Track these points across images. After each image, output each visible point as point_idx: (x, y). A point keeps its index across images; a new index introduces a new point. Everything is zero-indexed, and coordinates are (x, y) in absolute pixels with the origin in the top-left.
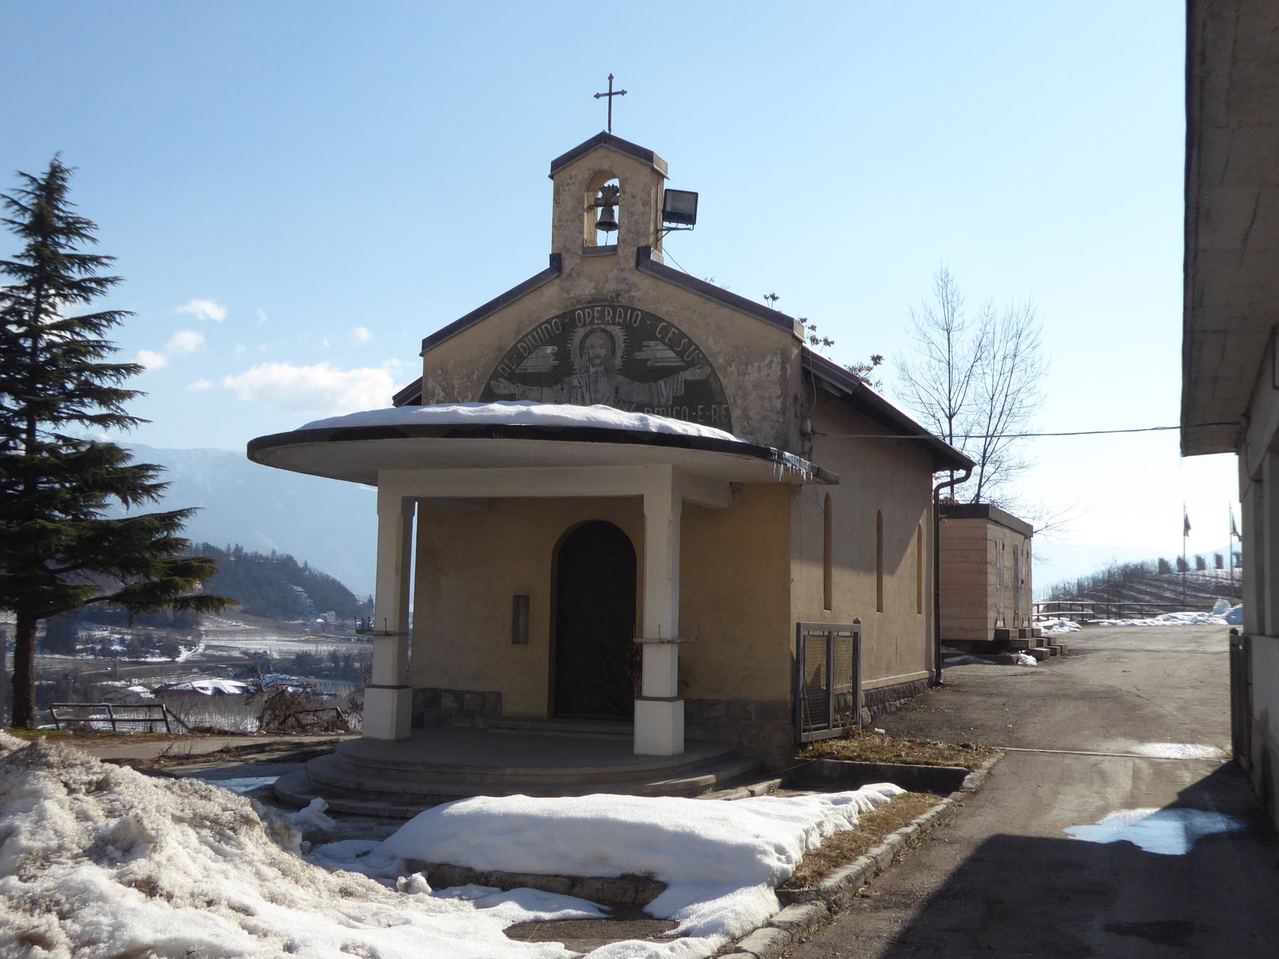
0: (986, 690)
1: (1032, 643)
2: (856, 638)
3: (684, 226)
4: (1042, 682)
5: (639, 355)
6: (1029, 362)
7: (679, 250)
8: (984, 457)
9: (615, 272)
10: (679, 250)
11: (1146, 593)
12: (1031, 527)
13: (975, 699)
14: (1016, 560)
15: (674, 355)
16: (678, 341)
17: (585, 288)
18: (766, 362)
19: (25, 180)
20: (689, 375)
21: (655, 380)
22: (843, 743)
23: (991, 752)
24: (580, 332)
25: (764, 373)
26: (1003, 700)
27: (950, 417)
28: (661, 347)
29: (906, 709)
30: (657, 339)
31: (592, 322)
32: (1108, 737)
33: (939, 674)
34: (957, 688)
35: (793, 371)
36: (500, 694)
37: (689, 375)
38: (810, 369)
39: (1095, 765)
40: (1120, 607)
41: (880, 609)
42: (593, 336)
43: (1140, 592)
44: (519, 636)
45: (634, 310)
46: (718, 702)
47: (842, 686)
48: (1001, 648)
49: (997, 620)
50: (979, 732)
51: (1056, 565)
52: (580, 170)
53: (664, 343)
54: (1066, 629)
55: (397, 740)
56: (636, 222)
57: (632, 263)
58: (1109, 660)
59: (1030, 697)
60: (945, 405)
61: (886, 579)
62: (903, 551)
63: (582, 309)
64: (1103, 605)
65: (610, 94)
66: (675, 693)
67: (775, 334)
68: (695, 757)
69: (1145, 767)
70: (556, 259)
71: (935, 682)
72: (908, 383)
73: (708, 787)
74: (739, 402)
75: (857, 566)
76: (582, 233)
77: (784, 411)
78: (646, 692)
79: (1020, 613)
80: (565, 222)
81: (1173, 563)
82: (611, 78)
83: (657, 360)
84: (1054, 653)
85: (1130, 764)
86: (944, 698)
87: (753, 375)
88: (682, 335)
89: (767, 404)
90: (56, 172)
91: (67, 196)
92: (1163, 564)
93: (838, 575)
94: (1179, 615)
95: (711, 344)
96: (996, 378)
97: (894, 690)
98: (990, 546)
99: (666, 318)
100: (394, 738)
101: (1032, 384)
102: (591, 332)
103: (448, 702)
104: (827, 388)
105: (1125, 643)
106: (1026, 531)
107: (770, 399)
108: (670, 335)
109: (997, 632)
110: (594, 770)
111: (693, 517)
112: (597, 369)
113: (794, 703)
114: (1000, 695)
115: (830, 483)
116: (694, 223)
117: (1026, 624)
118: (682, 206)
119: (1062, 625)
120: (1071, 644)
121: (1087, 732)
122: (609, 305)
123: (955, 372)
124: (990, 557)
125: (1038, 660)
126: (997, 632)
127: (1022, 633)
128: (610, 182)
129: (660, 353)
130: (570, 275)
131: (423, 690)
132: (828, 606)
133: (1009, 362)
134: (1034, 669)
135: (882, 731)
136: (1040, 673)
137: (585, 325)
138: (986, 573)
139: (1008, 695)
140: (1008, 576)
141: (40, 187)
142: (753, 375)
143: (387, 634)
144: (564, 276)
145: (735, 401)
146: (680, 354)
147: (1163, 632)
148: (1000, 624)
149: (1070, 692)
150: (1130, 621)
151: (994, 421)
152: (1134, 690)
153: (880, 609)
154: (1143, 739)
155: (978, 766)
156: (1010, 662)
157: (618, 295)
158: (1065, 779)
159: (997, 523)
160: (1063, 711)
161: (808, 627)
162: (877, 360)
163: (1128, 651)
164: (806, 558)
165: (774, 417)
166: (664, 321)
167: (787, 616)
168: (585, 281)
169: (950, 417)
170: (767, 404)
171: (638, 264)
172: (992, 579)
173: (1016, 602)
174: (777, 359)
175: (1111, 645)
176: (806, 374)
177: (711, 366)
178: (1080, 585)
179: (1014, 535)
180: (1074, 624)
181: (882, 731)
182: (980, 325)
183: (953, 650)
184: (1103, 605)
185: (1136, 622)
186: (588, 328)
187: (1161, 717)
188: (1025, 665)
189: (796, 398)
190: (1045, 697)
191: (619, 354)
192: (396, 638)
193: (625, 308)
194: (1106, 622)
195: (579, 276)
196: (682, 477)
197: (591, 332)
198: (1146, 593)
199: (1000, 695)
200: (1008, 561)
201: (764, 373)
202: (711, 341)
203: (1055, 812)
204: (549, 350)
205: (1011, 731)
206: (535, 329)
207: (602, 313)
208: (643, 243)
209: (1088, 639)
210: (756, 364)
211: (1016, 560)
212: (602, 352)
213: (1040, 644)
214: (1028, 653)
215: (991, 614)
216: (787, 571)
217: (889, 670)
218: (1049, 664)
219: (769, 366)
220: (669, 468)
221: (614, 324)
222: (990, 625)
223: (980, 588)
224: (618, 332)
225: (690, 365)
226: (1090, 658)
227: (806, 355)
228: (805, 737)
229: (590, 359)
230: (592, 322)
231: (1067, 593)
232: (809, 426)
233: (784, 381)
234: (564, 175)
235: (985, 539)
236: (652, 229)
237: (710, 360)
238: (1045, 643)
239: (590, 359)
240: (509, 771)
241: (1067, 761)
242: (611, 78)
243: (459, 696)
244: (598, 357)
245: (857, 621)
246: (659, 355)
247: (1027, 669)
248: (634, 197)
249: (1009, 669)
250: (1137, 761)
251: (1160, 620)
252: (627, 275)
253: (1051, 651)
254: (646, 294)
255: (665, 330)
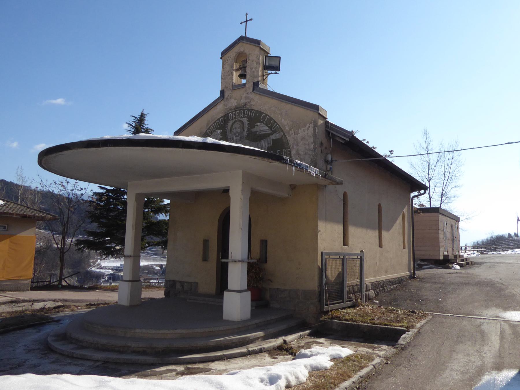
0: (433, 280)
1: (458, 260)
2: (361, 260)
3: (275, 72)
4: (459, 277)
5: (253, 130)
6: (458, 161)
7: (274, 83)
8: (442, 195)
9: (245, 95)
10: (274, 83)
11: (504, 244)
12: (459, 218)
13: (428, 285)
14: (452, 230)
15: (267, 128)
16: (271, 123)
17: (233, 103)
18: (307, 127)
19: (133, 118)
20: (273, 137)
21: (260, 141)
22: (351, 310)
23: (425, 315)
24: (231, 122)
25: (306, 132)
26: (440, 285)
27: (429, 181)
28: (263, 125)
29: (395, 289)
30: (261, 122)
31: (235, 118)
32: (487, 307)
33: (414, 273)
34: (422, 280)
35: (321, 132)
36: (197, 283)
37: (273, 137)
38: (330, 130)
39: (479, 326)
40: (495, 248)
41: (380, 246)
42: (236, 124)
43: (503, 243)
44: (205, 259)
45: (252, 110)
46: (285, 290)
47: (352, 281)
48: (445, 263)
49: (443, 252)
50: (424, 303)
51: (471, 233)
52: (232, 54)
53: (264, 123)
54: (475, 255)
55: (131, 306)
56: (254, 72)
57: (251, 89)
58: (490, 267)
59: (453, 284)
60: (427, 177)
61: (384, 234)
62: (394, 222)
63: (231, 112)
64: (487, 247)
65: (246, 21)
66: (245, 287)
67: (311, 114)
68: (255, 321)
69: (506, 327)
70: (222, 93)
71: (412, 277)
72: (414, 170)
73: (257, 339)
74: (295, 147)
75: (367, 226)
76: (232, 80)
77: (314, 150)
78: (230, 287)
79: (455, 249)
80: (226, 76)
81: (513, 235)
82: (247, 14)
83: (261, 131)
84: (468, 264)
85: (499, 326)
86: (415, 284)
87: (301, 134)
88: (271, 119)
89: (307, 147)
90: (142, 115)
91: (146, 122)
92: (510, 235)
93: (352, 230)
94: (517, 250)
95: (284, 122)
96: (446, 167)
97: (390, 282)
98: (440, 224)
99: (265, 112)
100: (129, 305)
101: (459, 169)
102: (235, 122)
103: (178, 286)
104: (338, 139)
105: (497, 260)
106: (457, 219)
107: (308, 144)
108: (266, 119)
109: (444, 256)
110: (184, 331)
111: (257, 199)
112: (237, 138)
113: (320, 292)
114: (439, 283)
115: (338, 183)
116: (279, 71)
117: (457, 253)
118: (274, 63)
119: (474, 254)
120: (476, 261)
121: (476, 304)
122: (242, 109)
123: (430, 166)
124: (440, 228)
125: (461, 267)
126: (444, 256)
127: (455, 257)
128: (248, 59)
129: (262, 128)
130: (227, 99)
131: (170, 281)
132: (345, 243)
133: (450, 161)
134: (458, 271)
135: (377, 302)
136: (460, 273)
137: (232, 119)
138: (439, 234)
139: (443, 283)
140: (449, 235)
141: (138, 120)
142: (301, 134)
143: (130, 256)
144: (225, 99)
145: (293, 147)
146: (270, 128)
147: (510, 256)
148: (446, 253)
149: (471, 282)
150: (499, 252)
151: (445, 182)
152: (500, 281)
153: (380, 246)
154: (506, 308)
155: (413, 327)
156: (449, 268)
157: (246, 104)
158: (460, 339)
159: (443, 215)
160: (468, 291)
161: (329, 254)
162: (391, 151)
163: (498, 263)
164: (328, 219)
165: (310, 153)
166: (263, 113)
167: (316, 249)
168: (233, 100)
169: (429, 181)
170: (307, 147)
171: (253, 90)
172: (441, 236)
173: (453, 245)
174: (312, 125)
175: (492, 261)
176: (328, 133)
177: (283, 131)
178: (482, 242)
179: (451, 220)
180: (478, 253)
181: (377, 302)
182: (439, 148)
183: (426, 263)
184: (489, 247)
185: (502, 252)
186: (234, 120)
187: (514, 295)
188: (455, 269)
189: (321, 144)
190: (461, 283)
191: (246, 130)
192: (132, 259)
193: (248, 110)
194: (490, 253)
195: (231, 98)
196: (248, 178)
197: (235, 122)
198: (504, 244)
199: (439, 283)
200: (448, 230)
201: (306, 132)
202: (283, 120)
203: (447, 373)
204: (219, 131)
205: (440, 302)
206: (214, 123)
207: (239, 113)
208: (256, 80)
209: (483, 259)
210: (302, 129)
211: (452, 230)
212: (239, 130)
213: (462, 261)
214: (457, 265)
215: (442, 249)
216: (316, 226)
217: (386, 272)
218: (465, 269)
219: (308, 129)
220: (240, 172)
221: (244, 117)
222: (441, 253)
223: (437, 239)
224: (245, 120)
225: (274, 132)
226: (483, 266)
227: (328, 125)
228: (326, 308)
229: (235, 134)
230: (235, 118)
231: (478, 244)
232: (329, 158)
233: (315, 135)
234: (226, 56)
235: (438, 221)
236: (260, 74)
237: (283, 128)
238: (465, 260)
239: (235, 134)
240: (138, 331)
241: (465, 323)
242: (247, 14)
243: (182, 283)
244: (237, 132)
245: (362, 251)
246: (262, 129)
247: (455, 271)
248: (253, 61)
249: (448, 271)
250: (503, 323)
251: (510, 252)
252: (249, 95)
253: (467, 263)
254: (258, 103)
255: (264, 117)
